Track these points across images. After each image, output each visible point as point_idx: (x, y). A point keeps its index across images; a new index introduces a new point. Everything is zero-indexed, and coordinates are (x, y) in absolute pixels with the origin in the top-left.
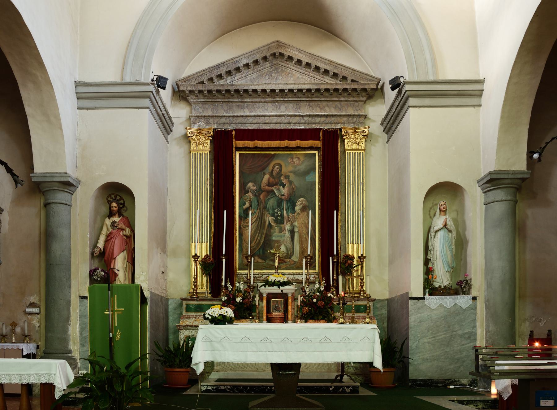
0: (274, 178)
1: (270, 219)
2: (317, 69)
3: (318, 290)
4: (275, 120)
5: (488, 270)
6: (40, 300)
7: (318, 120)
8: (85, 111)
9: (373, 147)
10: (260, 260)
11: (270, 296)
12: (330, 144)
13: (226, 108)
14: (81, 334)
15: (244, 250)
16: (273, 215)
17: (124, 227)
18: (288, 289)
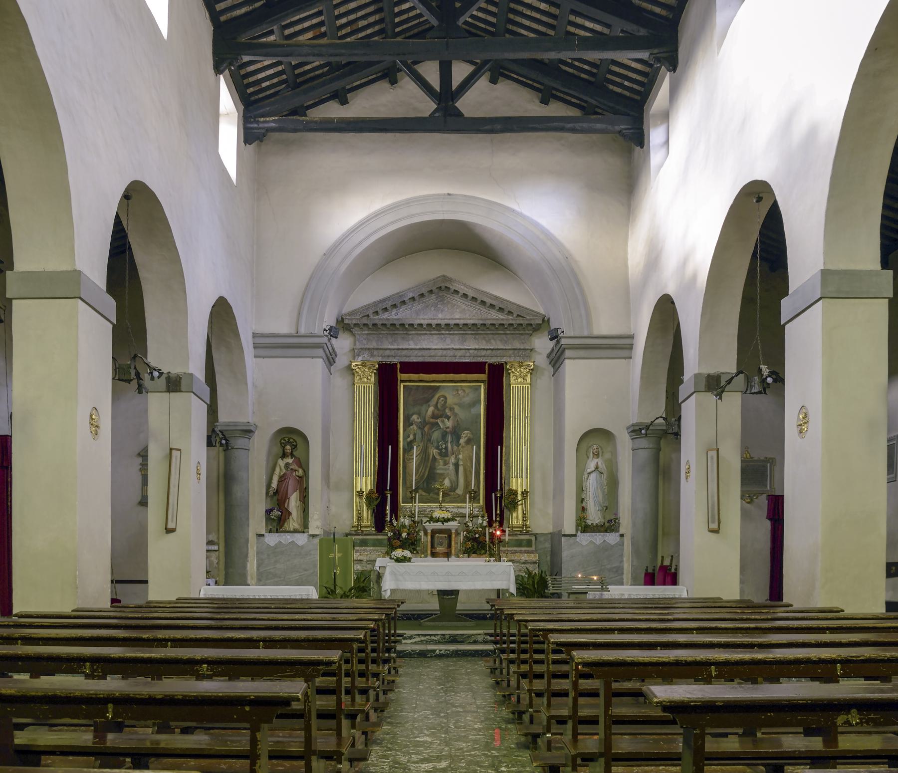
0: (438, 410)
1: (434, 452)
2: (483, 303)
3: (481, 525)
4: (440, 353)
5: (634, 511)
6: (218, 538)
7: (483, 353)
8: (261, 359)
9: (539, 381)
10: (424, 494)
11: (434, 532)
12: (496, 377)
13: (390, 340)
14: (258, 569)
15: (408, 483)
16: (437, 448)
17: (297, 468)
18: (453, 525)
